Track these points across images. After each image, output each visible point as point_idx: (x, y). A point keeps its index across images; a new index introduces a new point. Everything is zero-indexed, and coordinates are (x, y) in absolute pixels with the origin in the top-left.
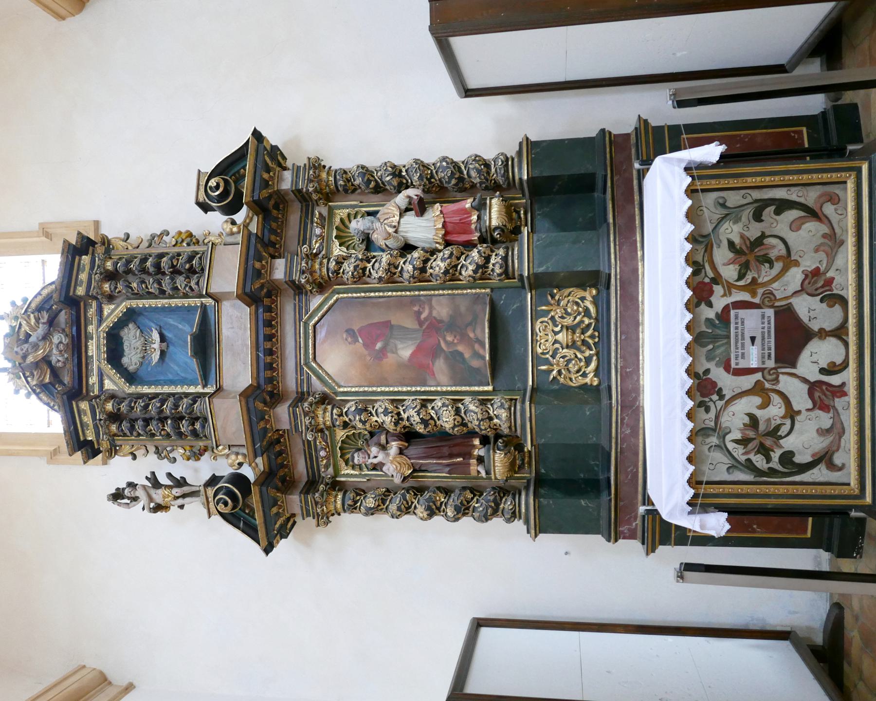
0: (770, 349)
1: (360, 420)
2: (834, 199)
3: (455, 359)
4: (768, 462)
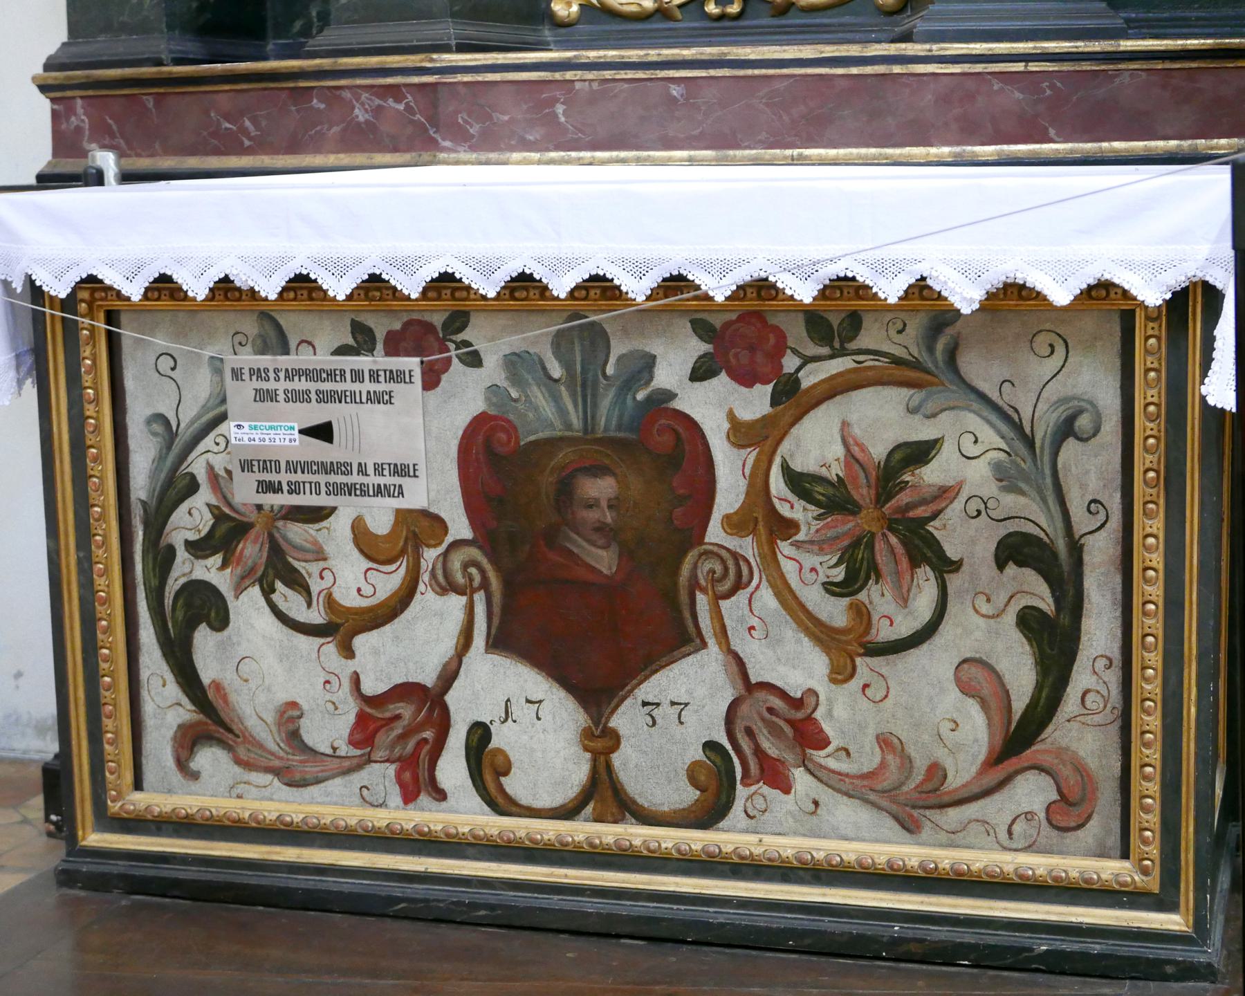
0: (294, 489)
2: (1067, 812)
4: (189, 545)
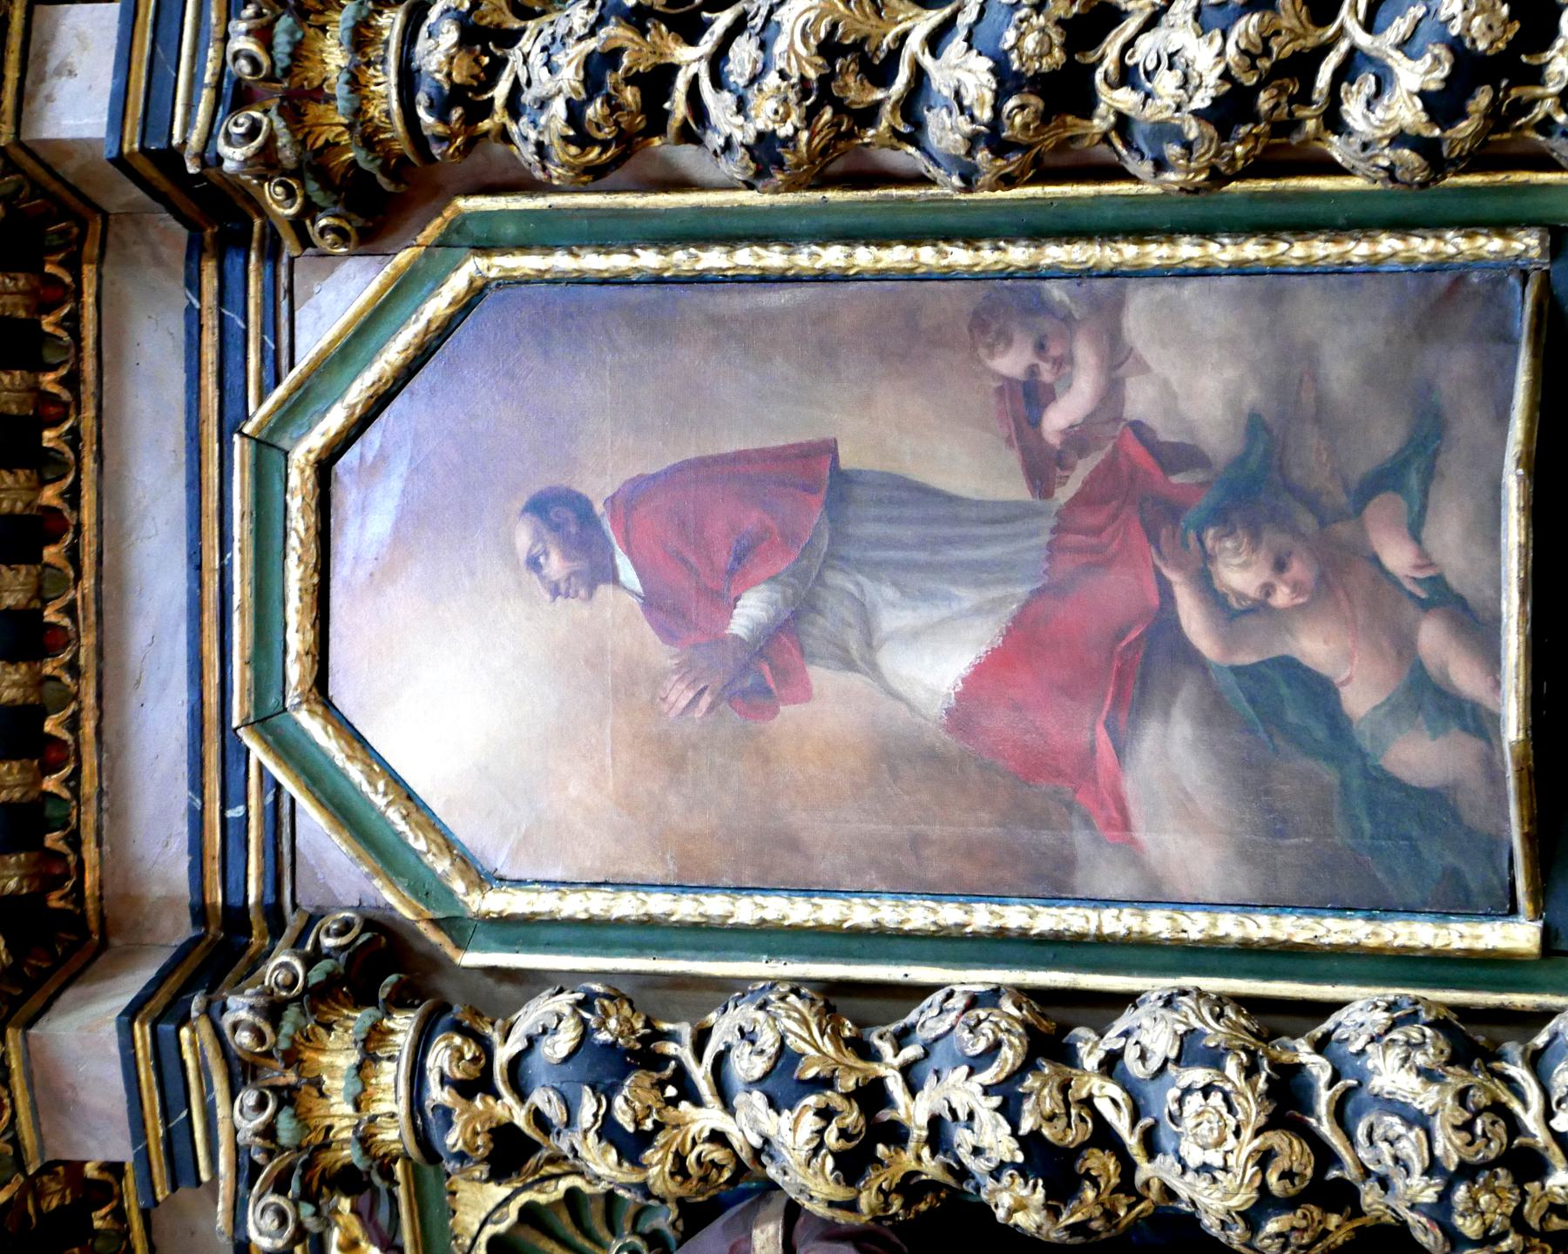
1: (608, 1130)
3: (1276, 711)
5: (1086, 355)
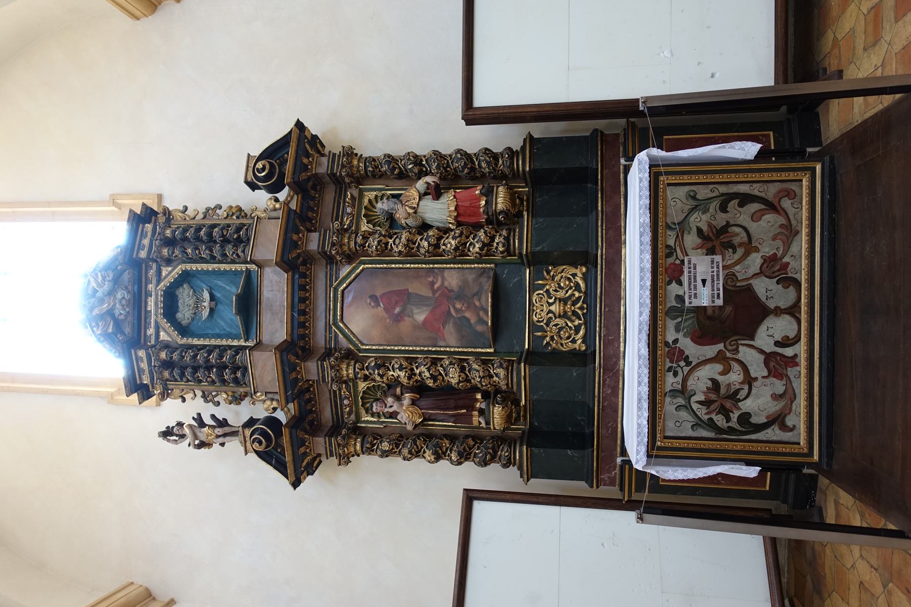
1: (379, 374)
2: (791, 195)
4: (727, 422)
5: (440, 279)
